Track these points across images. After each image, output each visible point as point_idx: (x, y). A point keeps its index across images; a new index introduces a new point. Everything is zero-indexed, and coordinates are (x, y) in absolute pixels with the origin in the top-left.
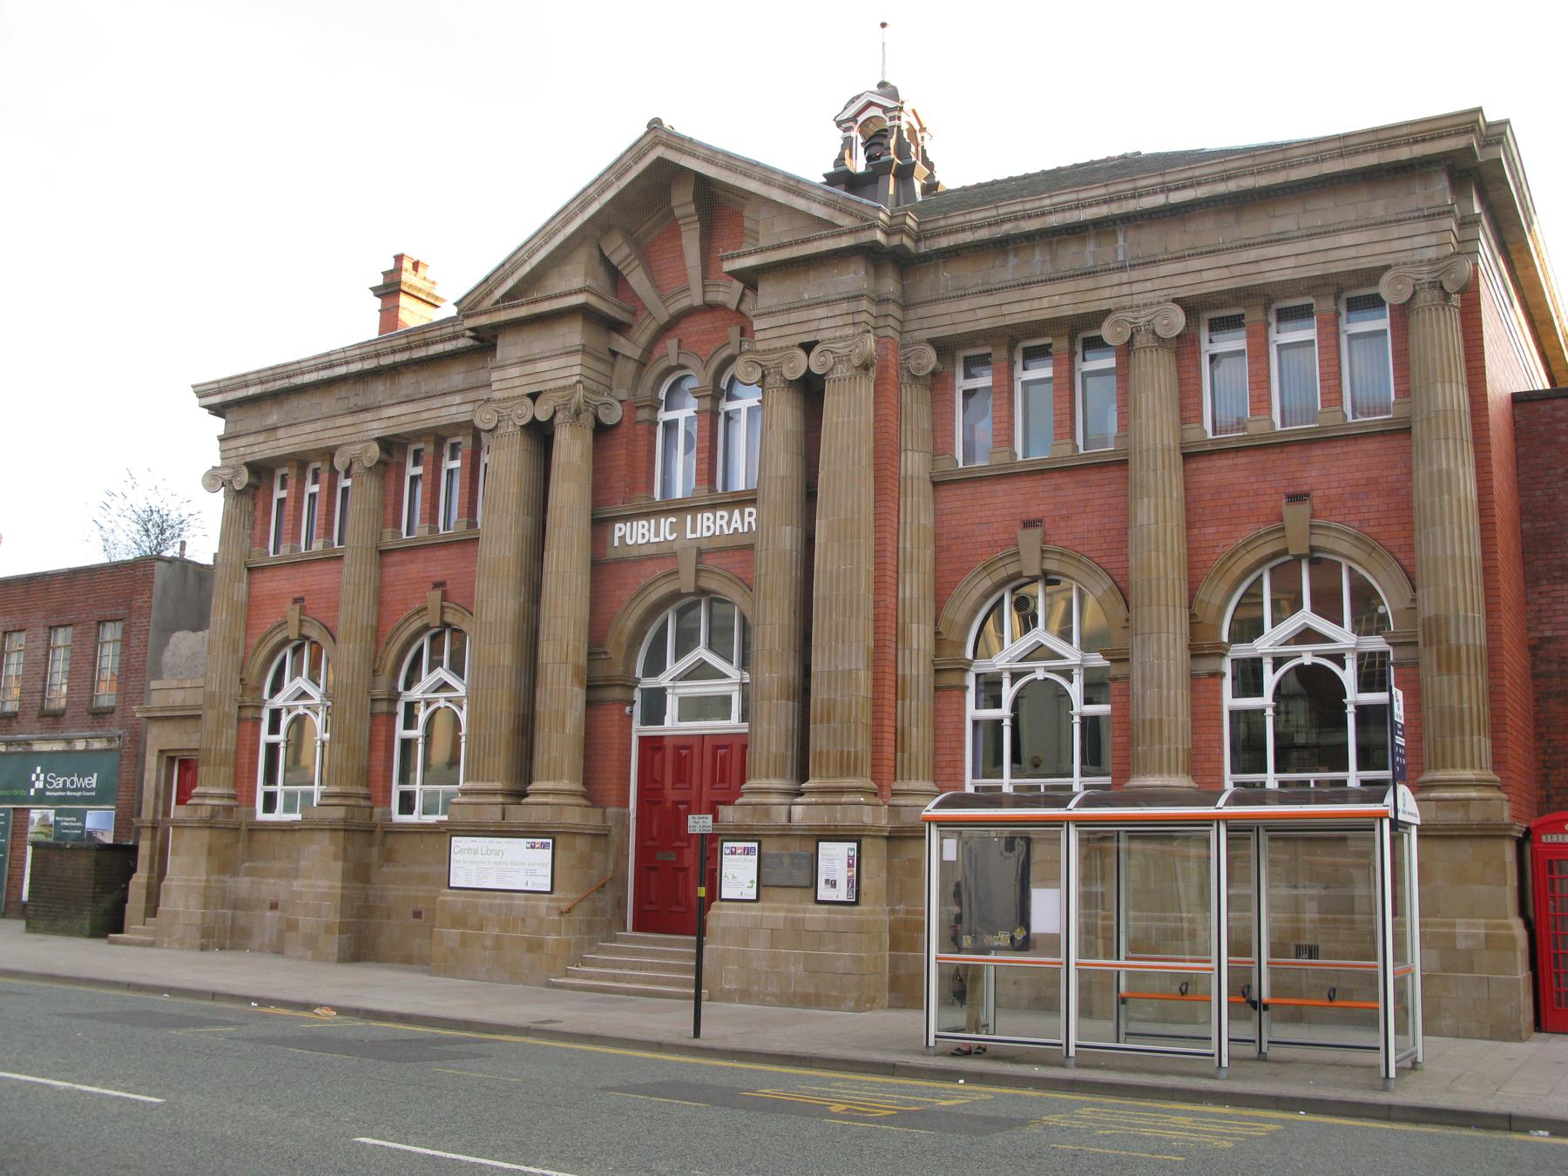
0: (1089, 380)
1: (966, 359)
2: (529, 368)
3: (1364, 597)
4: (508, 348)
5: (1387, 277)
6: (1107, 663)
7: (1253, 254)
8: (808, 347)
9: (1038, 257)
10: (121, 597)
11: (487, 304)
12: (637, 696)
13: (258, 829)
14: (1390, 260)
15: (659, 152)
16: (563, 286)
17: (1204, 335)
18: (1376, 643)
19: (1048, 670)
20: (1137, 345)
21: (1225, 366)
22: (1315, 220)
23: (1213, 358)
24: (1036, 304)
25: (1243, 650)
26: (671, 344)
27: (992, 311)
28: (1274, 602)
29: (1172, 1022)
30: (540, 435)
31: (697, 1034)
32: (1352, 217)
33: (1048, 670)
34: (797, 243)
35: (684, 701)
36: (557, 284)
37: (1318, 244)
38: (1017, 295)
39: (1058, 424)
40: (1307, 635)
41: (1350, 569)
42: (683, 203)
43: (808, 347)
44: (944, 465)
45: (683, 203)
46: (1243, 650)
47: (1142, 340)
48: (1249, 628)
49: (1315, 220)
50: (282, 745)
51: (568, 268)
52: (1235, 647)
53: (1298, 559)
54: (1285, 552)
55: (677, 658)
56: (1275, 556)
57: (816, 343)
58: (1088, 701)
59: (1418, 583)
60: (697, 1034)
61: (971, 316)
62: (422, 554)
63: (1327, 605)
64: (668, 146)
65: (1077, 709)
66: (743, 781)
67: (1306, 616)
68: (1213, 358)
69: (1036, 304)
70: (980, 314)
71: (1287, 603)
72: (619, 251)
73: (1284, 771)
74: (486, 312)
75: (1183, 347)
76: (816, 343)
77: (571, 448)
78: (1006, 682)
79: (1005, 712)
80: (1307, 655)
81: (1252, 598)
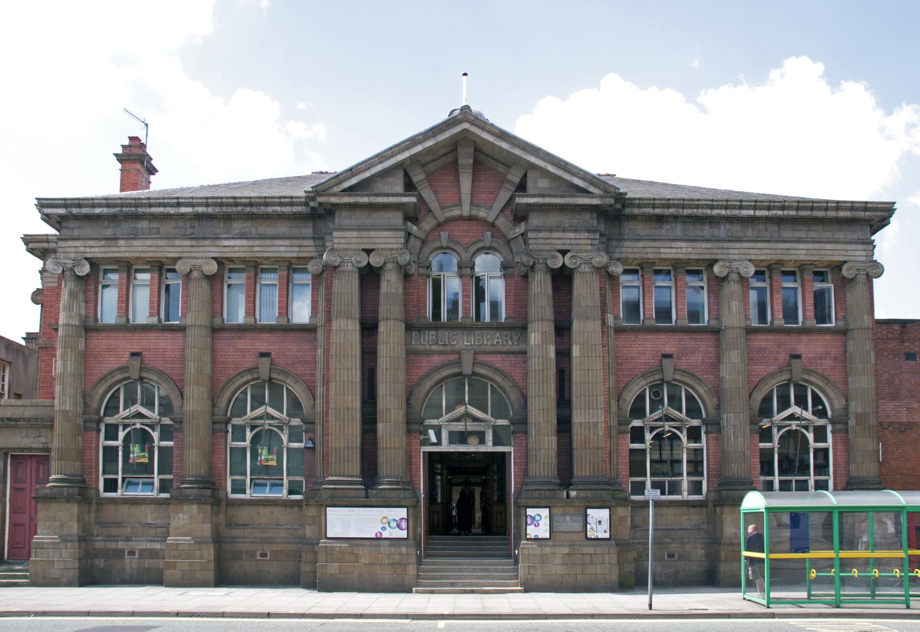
0: (793, 291)
1: (104, 270)
2: (364, 234)
3: (817, 400)
4: (341, 218)
5: (845, 267)
7: (787, 245)
10: (8, 344)
11: (336, 189)
12: (230, 429)
13: (102, 502)
14: (181, 255)
17: (226, 274)
19: (142, 424)
23: (229, 286)
26: (444, 235)
27: (654, 250)
28: (125, 400)
30: (370, 277)
32: (856, 237)
33: (142, 424)
34: (550, 196)
35: (451, 434)
37: (817, 246)
38: (668, 244)
39: (151, 308)
40: (792, 417)
41: (686, 390)
42: (466, 160)
43: (564, 253)
44: (218, 321)
45: (466, 160)
46: (236, 421)
47: (195, 274)
48: (112, 408)
49: (798, 234)
52: (234, 419)
53: (264, 381)
54: (258, 378)
55: (252, 409)
57: (569, 251)
59: (185, 397)
62: (249, 335)
63: (801, 402)
64: (472, 124)
68: (229, 286)
71: (258, 401)
72: (418, 177)
73: (819, 475)
75: (214, 281)
77: (390, 283)
78: (121, 428)
79: (119, 443)
80: (794, 425)
81: (115, 397)
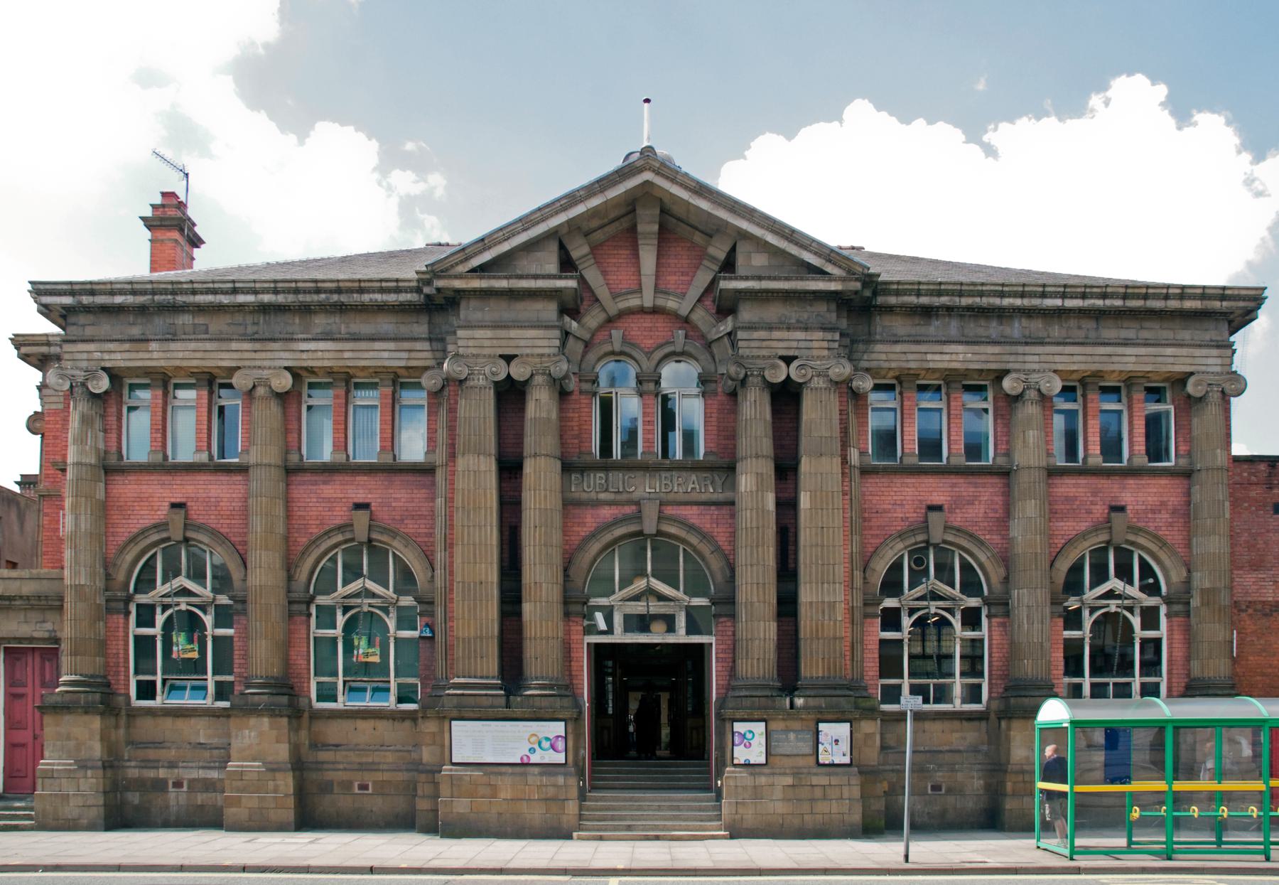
3: (1146, 570)
6: (231, 602)
7: (1108, 350)
8: (788, 360)
9: (1017, 325)
11: (461, 269)
12: (313, 610)
15: (648, 176)
16: (534, 269)
17: (305, 390)
18: (973, 602)
19: (188, 604)
20: (1027, 397)
21: (316, 416)
22: (1145, 334)
24: (954, 357)
25: (143, 599)
29: (434, 827)
30: (510, 395)
31: (907, 860)
32: (1208, 337)
33: (188, 604)
34: (769, 278)
35: (627, 618)
36: (528, 264)
41: (961, 557)
42: (648, 226)
43: (788, 360)
45: (648, 226)
46: (143, 599)
48: (146, 582)
50: (906, 641)
51: (539, 254)
52: (138, 596)
53: (361, 544)
54: (352, 540)
56: (346, 541)
57: (795, 358)
58: (1144, 628)
60: (907, 860)
61: (903, 357)
64: (658, 173)
65: (209, 632)
66: (58, 677)
67: (183, 581)
68: (309, 408)
69: (954, 357)
70: (910, 357)
71: (172, 571)
74: (459, 277)
76: (795, 358)
78: (159, 610)
80: (1113, 605)
